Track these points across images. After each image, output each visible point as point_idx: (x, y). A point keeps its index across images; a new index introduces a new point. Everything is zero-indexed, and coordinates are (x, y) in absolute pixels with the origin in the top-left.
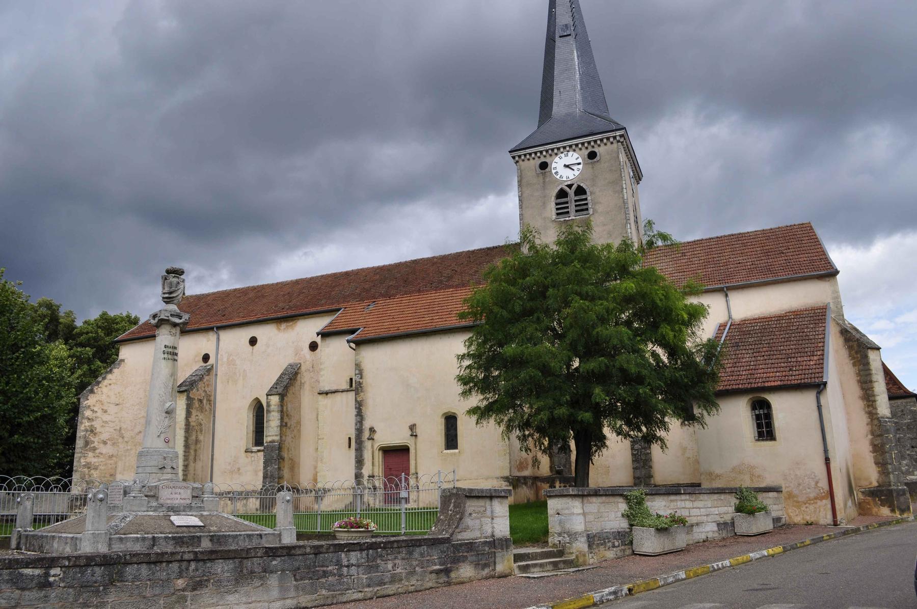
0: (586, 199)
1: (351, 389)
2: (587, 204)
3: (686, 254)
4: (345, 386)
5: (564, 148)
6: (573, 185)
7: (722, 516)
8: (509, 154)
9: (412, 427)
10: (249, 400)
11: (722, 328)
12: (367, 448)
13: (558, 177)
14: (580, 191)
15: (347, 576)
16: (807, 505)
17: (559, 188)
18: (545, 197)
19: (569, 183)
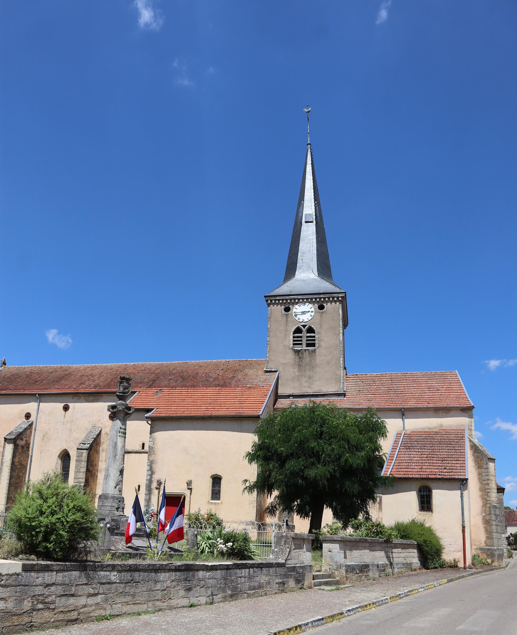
0: (314, 337)
1: (143, 451)
2: (314, 340)
3: (376, 382)
4: (139, 448)
5: (303, 299)
6: (306, 325)
7: (405, 558)
8: (264, 298)
9: (189, 483)
10: (58, 451)
11: (399, 435)
12: (154, 494)
13: (297, 319)
14: (311, 330)
15: (240, 583)
16: (449, 555)
17: (296, 327)
18: (286, 331)
19: (304, 324)
